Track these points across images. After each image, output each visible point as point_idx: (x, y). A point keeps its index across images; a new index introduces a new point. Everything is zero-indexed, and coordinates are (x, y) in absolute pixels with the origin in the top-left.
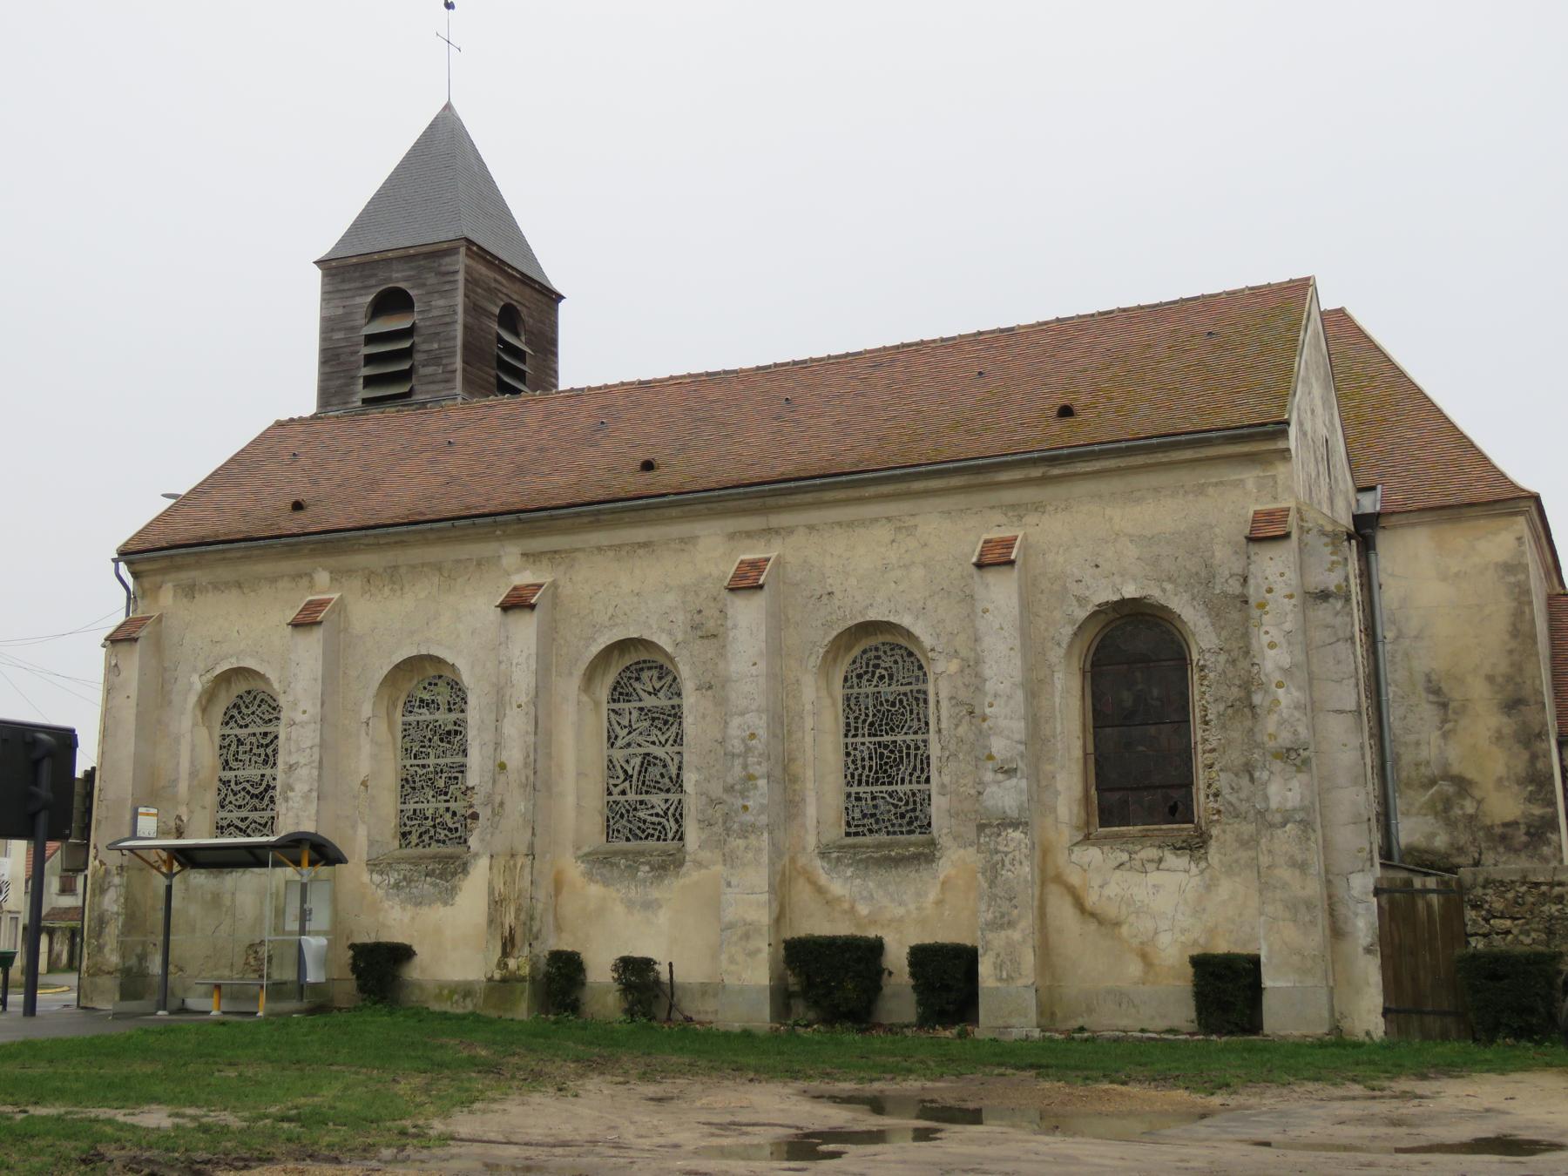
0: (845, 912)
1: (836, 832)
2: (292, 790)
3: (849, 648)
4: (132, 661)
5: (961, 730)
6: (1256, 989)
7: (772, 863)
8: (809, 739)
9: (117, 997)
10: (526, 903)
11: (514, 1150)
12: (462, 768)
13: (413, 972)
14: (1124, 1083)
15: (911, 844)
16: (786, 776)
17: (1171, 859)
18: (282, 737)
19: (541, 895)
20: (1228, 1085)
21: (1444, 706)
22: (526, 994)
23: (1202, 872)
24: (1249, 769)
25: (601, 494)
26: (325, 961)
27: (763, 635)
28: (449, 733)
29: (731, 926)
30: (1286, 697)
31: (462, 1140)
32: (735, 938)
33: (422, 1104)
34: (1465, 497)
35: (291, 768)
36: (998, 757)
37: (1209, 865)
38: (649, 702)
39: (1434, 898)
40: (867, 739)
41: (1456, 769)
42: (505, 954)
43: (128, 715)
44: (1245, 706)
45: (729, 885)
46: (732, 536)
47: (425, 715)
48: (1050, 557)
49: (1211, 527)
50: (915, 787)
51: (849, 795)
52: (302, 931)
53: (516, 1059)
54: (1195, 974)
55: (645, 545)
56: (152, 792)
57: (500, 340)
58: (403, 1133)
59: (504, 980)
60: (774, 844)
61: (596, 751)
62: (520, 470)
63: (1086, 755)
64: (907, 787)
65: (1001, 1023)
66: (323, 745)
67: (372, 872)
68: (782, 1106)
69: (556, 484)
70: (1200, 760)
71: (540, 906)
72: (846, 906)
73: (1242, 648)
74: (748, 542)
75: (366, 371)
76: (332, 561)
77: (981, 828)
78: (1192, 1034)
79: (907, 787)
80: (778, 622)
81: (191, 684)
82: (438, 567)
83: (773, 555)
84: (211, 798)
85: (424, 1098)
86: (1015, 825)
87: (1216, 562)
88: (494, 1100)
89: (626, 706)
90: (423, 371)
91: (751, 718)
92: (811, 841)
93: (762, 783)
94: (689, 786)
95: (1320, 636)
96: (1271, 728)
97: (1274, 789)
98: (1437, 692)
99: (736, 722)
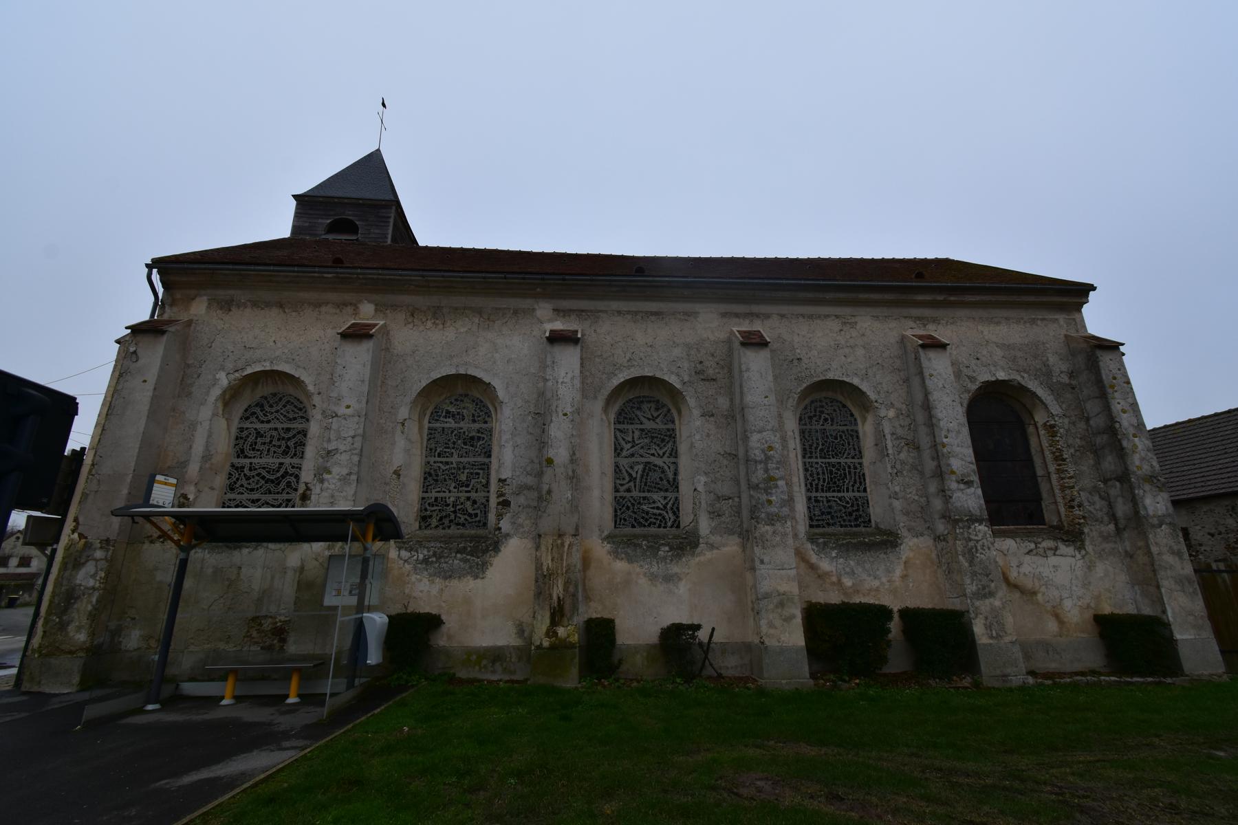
0: (833, 584)
2: (329, 472)
4: (154, 355)
5: (903, 456)
13: (441, 640)
22: (577, 660)
23: (1083, 557)
28: (472, 438)
32: (771, 606)
37: (1087, 553)
38: (649, 425)
39: (1225, 575)
40: (819, 460)
42: (554, 623)
43: (142, 396)
45: (762, 562)
46: (724, 315)
47: (450, 423)
50: (857, 494)
51: (809, 499)
55: (656, 314)
59: (553, 647)
64: (851, 494)
65: (998, 672)
67: (400, 549)
72: (834, 579)
74: (737, 320)
79: (851, 494)
81: (215, 381)
82: (479, 312)
84: (220, 480)
89: (630, 427)
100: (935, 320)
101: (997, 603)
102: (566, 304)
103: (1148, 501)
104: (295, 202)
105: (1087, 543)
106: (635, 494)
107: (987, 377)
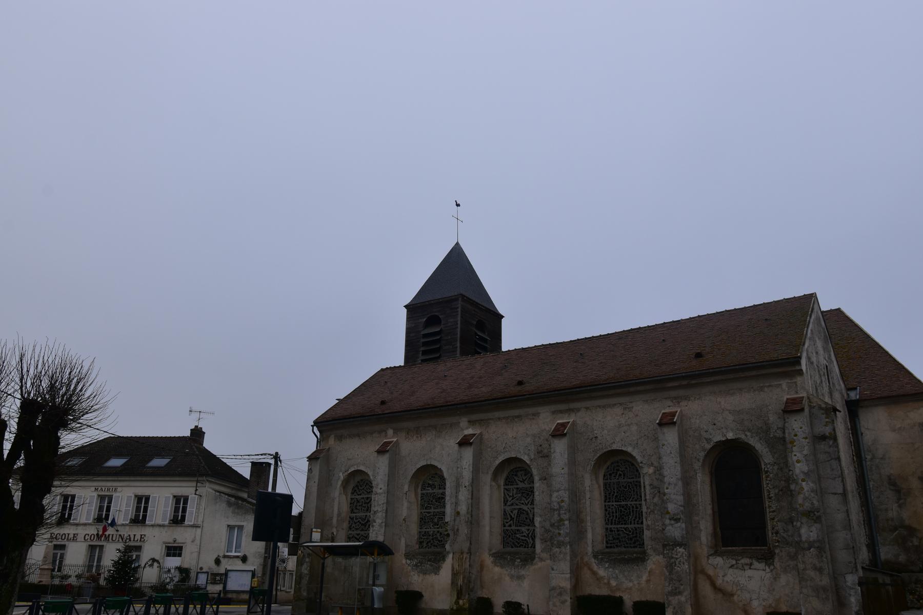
5: (656, 500)
23: (772, 571)
38: (521, 485)
39: (890, 588)
43: (315, 489)
46: (554, 413)
50: (637, 526)
51: (607, 529)
64: (633, 526)
72: (606, 581)
79: (633, 526)
84: (345, 525)
100: (687, 398)
101: (683, 599)
102: (474, 417)
103: (803, 531)
105: (776, 560)
106: (513, 528)
107: (719, 438)
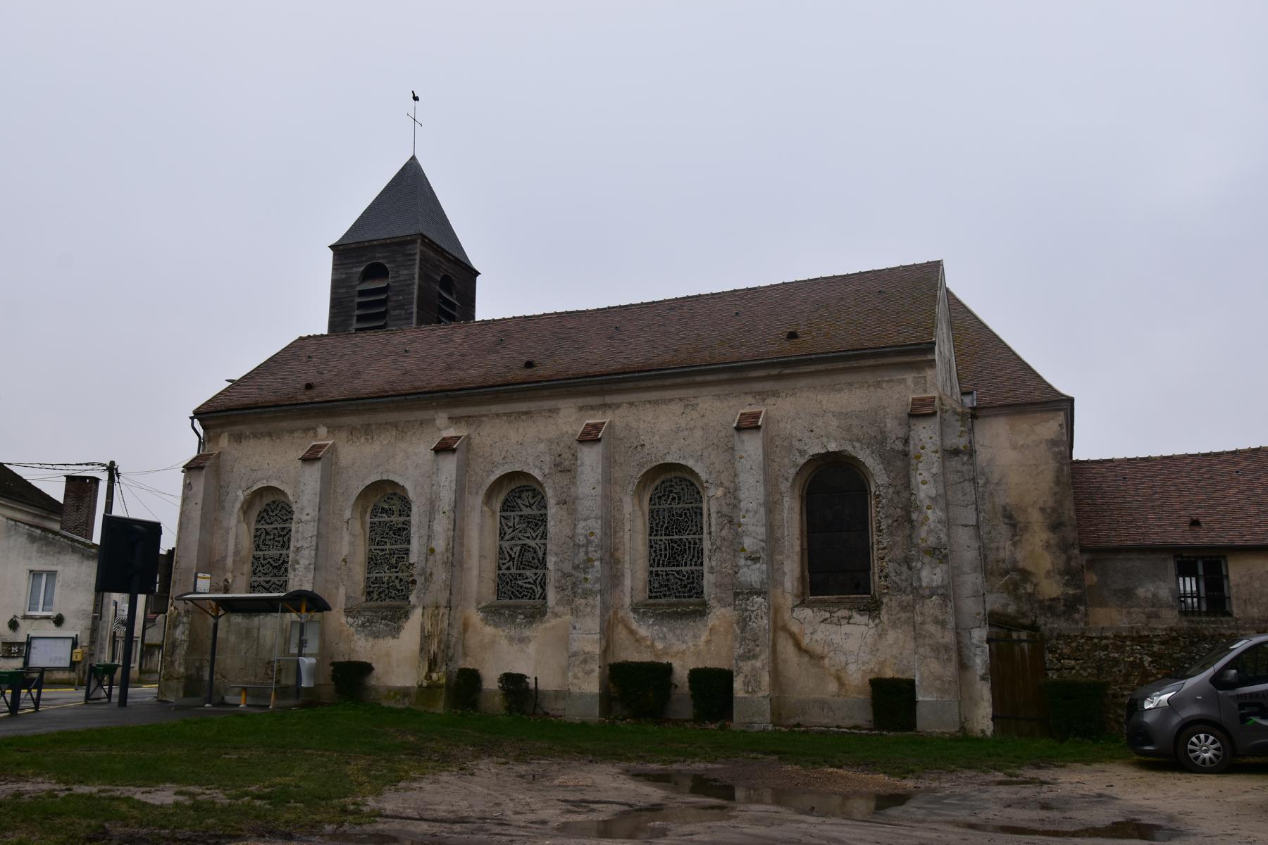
0: (648, 647)
1: (642, 596)
3: (653, 480)
4: (200, 483)
5: (724, 533)
6: (912, 702)
7: (602, 615)
8: (627, 536)
9: (181, 695)
10: (444, 638)
11: (424, 826)
12: (407, 552)
13: (372, 681)
14: (840, 767)
15: (691, 604)
16: (612, 559)
17: (857, 617)
18: (293, 530)
19: (455, 632)
20: (912, 771)
21: (1014, 526)
24: (907, 561)
25: (499, 380)
26: (314, 672)
27: (600, 470)
29: (575, 654)
30: (933, 515)
31: (387, 816)
33: (361, 784)
34: (1028, 399)
35: (298, 549)
36: (748, 550)
38: (526, 511)
39: (1026, 645)
41: (1021, 565)
42: (431, 670)
43: (196, 514)
44: (907, 518)
45: (575, 628)
46: (581, 409)
48: (782, 425)
49: (885, 408)
50: (693, 568)
51: (651, 573)
52: (300, 654)
53: (433, 745)
54: (873, 691)
55: (526, 413)
56: (209, 564)
57: (441, 296)
58: (344, 811)
59: (429, 687)
60: (603, 603)
61: (491, 542)
62: (449, 367)
63: (802, 549)
64: (688, 568)
65: (747, 720)
66: (319, 536)
68: (614, 785)
69: (472, 373)
70: (875, 554)
71: (454, 640)
72: (648, 643)
73: (905, 483)
75: (357, 312)
76: (329, 421)
77: (736, 595)
78: (870, 730)
79: (688, 568)
80: (609, 462)
82: (395, 425)
83: (607, 421)
84: (247, 568)
85: (364, 778)
86: (758, 593)
87: (887, 430)
88: (415, 780)
90: (393, 313)
91: (591, 522)
92: (627, 601)
93: (597, 564)
94: (550, 565)
95: (953, 477)
96: (923, 535)
97: (925, 574)
98: (1010, 517)
99: (581, 525)
102: (458, 412)
104: (331, 253)
106: (513, 571)
107: (817, 449)
